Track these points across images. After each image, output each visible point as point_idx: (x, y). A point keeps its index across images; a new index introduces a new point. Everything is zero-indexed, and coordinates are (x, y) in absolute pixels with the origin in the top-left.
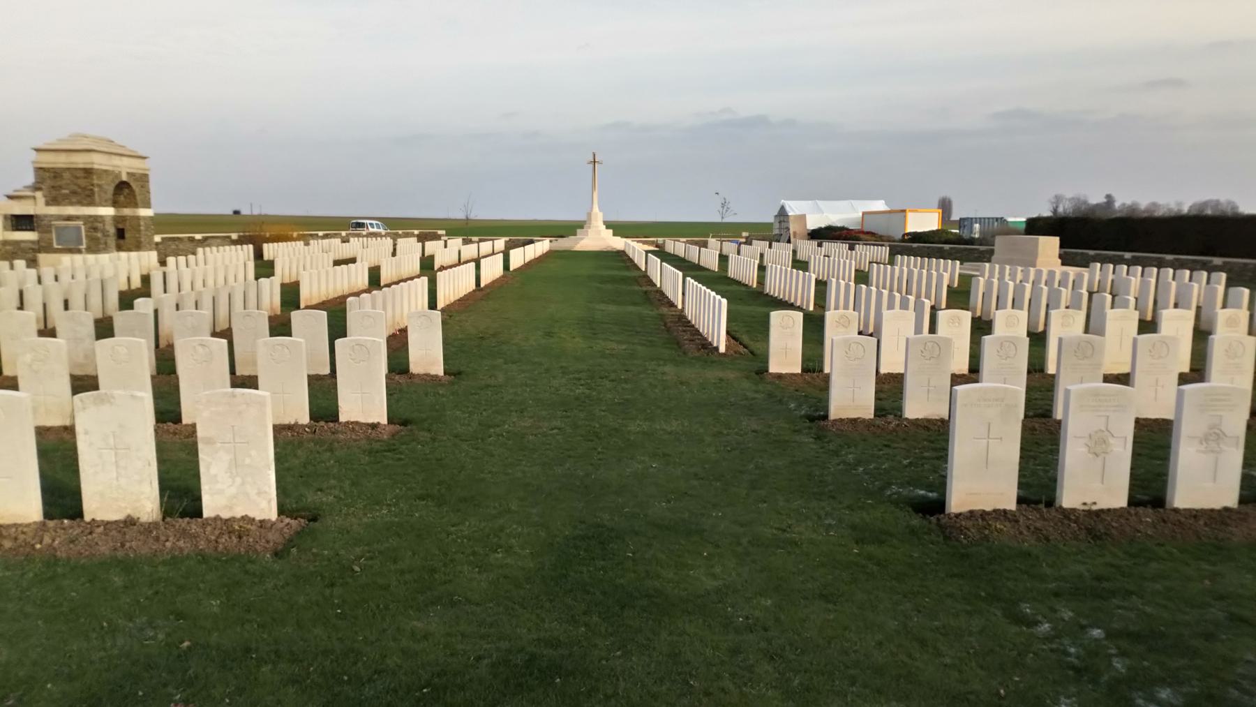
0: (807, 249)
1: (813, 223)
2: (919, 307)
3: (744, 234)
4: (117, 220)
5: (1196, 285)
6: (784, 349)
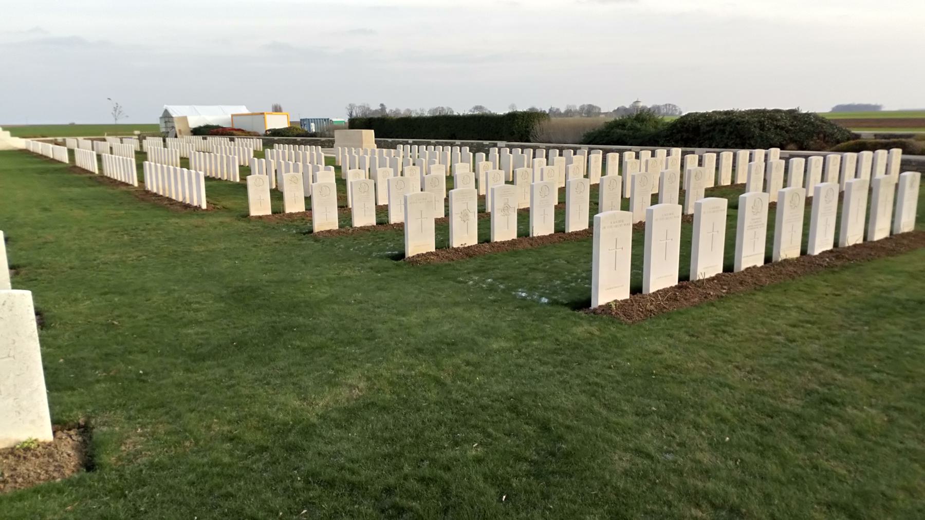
1: (194, 123)
6: (259, 205)
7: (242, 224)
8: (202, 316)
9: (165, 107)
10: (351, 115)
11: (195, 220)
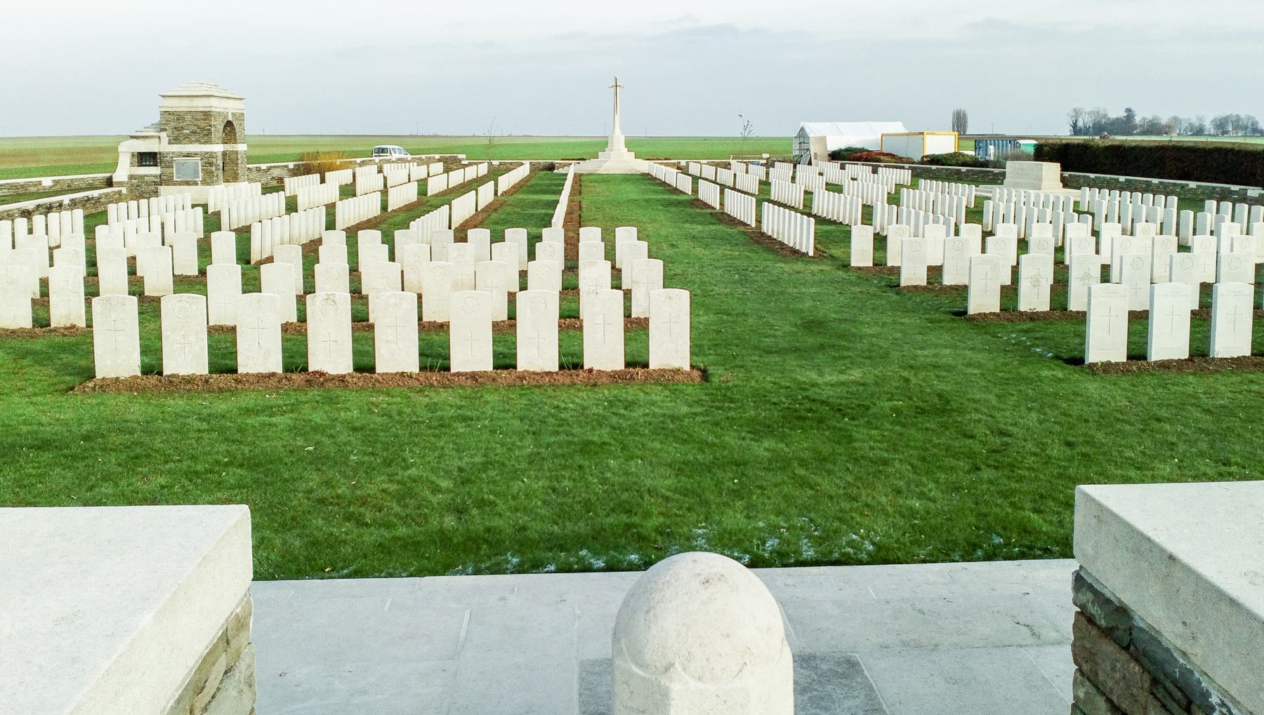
0: (833, 171)
1: (833, 146)
2: (946, 223)
3: (766, 156)
4: (224, 154)
5: (1144, 207)
6: (861, 253)
7: (841, 273)
8: (779, 333)
9: (802, 124)
10: (1075, 126)
11: (799, 266)
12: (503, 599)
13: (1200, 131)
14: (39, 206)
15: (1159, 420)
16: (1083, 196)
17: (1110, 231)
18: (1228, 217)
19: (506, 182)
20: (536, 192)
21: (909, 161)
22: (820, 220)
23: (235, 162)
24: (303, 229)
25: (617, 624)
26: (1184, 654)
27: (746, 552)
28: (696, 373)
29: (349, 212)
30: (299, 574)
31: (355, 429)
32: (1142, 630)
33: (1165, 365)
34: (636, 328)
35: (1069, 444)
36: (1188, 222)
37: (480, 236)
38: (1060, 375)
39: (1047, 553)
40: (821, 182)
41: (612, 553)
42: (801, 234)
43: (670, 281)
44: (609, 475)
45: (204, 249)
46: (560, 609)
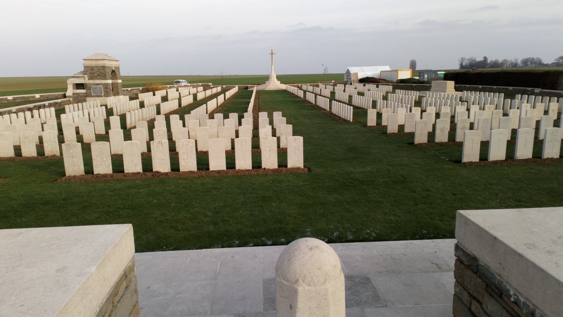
0: (360, 87)
1: (361, 76)
2: (406, 107)
3: (333, 81)
4: (112, 84)
6: (372, 120)
10: (461, 65)
12: (233, 257)
13: (515, 65)
14: (35, 106)
15: (491, 184)
16: (464, 94)
17: (474, 109)
18: (526, 101)
19: (229, 94)
20: (241, 98)
21: (392, 82)
22: (355, 108)
23: (117, 87)
24: (148, 115)
25: (277, 265)
26: (499, 275)
27: (326, 237)
28: (306, 169)
29: (166, 107)
30: (153, 250)
31: (173, 194)
32: (482, 266)
33: (495, 162)
34: (282, 153)
35: (454, 194)
36: (508, 104)
37: (219, 116)
38: (451, 167)
39: (444, 237)
40: (355, 92)
41: (275, 238)
42: (347, 113)
43: (295, 133)
44: (272, 209)
45: (107, 124)
46: (255, 260)
